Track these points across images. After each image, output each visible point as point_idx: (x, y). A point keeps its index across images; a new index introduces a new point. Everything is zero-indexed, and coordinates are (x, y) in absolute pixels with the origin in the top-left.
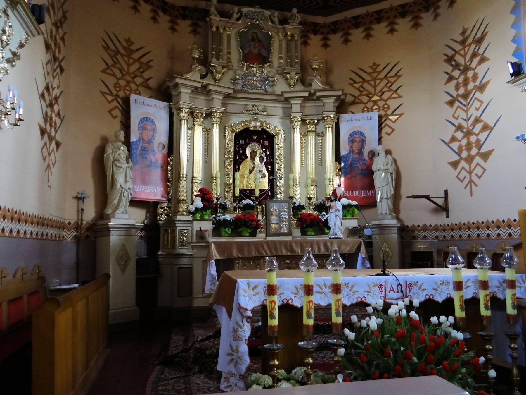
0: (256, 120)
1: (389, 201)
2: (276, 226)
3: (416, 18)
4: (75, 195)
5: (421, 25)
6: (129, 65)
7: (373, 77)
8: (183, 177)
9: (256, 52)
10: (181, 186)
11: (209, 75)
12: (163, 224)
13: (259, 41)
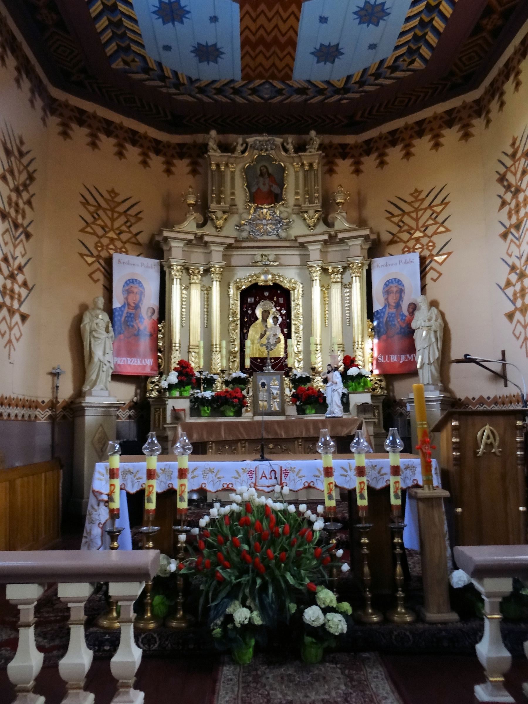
0: (266, 273)
1: (433, 367)
2: (265, 403)
3: (466, 126)
4: (50, 370)
5: (472, 135)
6: (113, 220)
7: (414, 207)
8: (175, 346)
9: (266, 189)
10: (173, 357)
11: (209, 223)
12: (153, 401)
13: (269, 175)
